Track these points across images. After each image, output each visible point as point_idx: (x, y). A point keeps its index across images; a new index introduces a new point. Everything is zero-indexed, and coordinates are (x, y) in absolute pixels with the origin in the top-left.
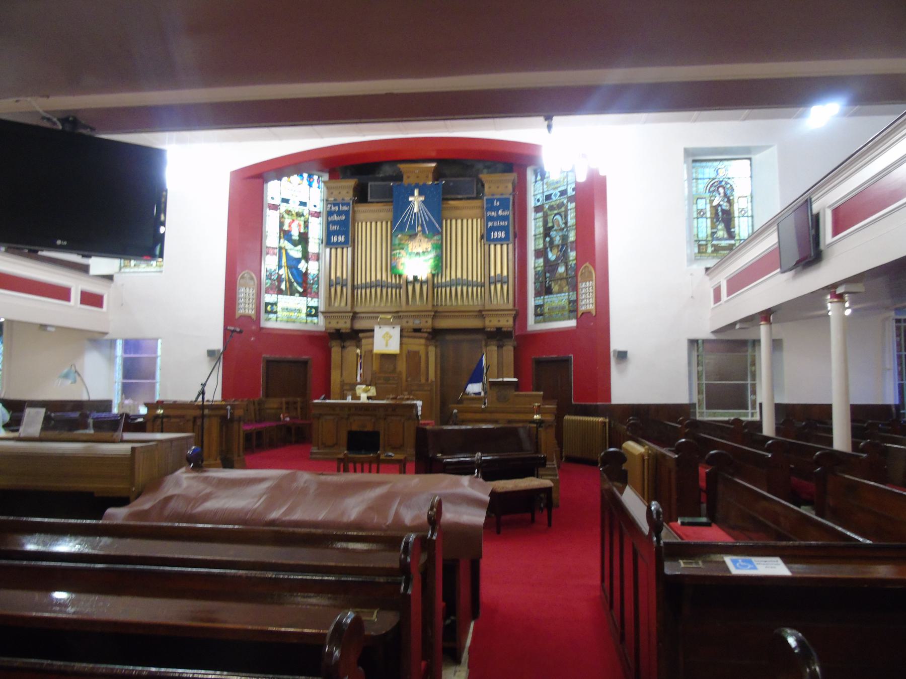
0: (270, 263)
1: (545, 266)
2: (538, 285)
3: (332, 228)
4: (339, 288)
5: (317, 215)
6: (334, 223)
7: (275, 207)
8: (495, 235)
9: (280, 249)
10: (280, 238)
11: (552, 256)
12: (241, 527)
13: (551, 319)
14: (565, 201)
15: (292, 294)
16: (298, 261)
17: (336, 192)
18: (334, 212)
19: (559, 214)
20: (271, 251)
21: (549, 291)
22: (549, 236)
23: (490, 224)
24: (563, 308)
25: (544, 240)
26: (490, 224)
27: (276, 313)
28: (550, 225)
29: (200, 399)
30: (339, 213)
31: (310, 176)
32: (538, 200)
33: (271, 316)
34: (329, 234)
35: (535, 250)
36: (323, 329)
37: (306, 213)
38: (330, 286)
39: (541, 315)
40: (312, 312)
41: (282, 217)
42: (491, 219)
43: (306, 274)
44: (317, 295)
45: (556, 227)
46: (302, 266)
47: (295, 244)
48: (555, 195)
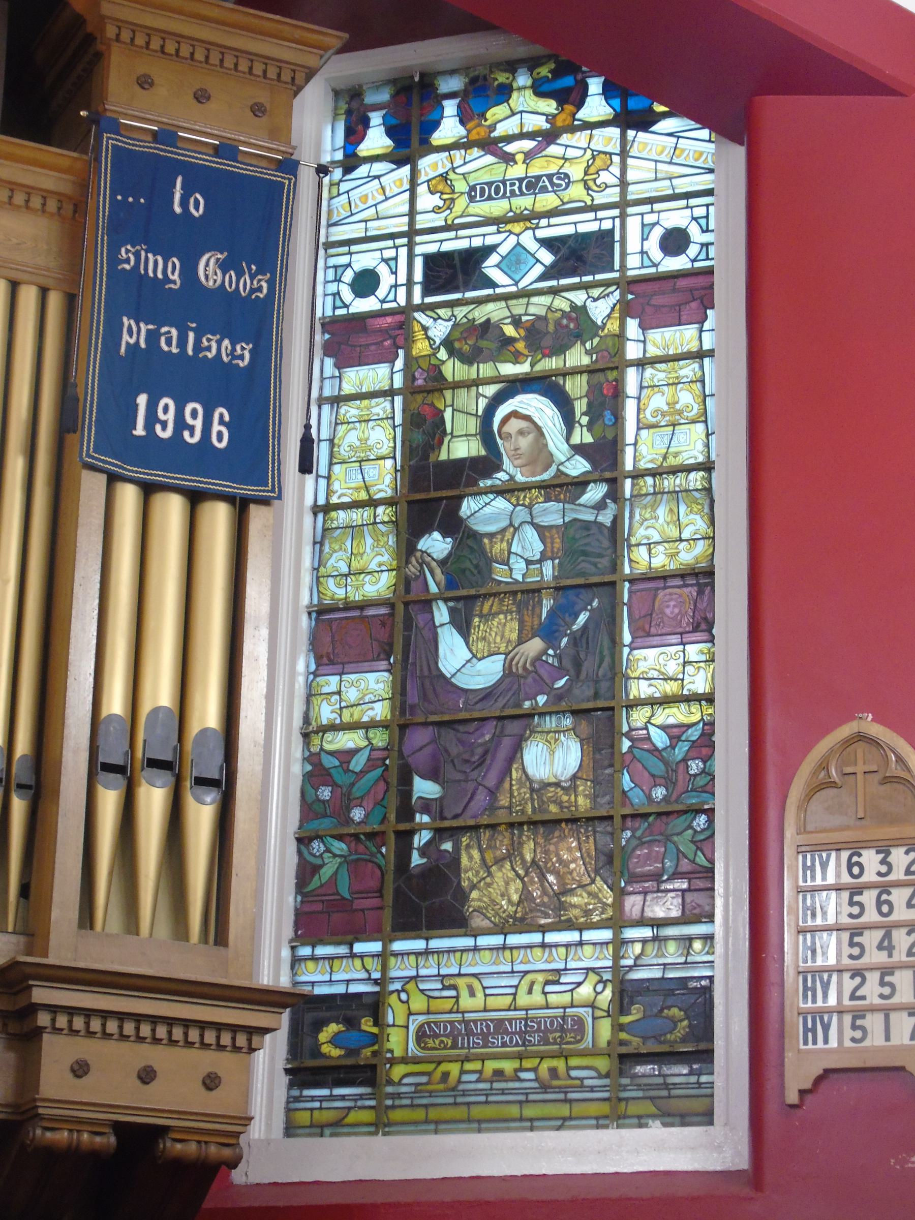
1: (402, 723)
2: (332, 855)
8: (162, 416)
11: (466, 661)
13: (447, 1108)
14: (599, 310)
19: (548, 386)
21: (429, 903)
22: (452, 525)
23: (134, 334)
24: (563, 1033)
25: (407, 549)
26: (134, 334)
28: (462, 448)
29: (456, 1007)
32: (366, 283)
35: (321, 612)
39: (364, 1072)
42: (141, 296)
45: (510, 470)
48: (515, 260)
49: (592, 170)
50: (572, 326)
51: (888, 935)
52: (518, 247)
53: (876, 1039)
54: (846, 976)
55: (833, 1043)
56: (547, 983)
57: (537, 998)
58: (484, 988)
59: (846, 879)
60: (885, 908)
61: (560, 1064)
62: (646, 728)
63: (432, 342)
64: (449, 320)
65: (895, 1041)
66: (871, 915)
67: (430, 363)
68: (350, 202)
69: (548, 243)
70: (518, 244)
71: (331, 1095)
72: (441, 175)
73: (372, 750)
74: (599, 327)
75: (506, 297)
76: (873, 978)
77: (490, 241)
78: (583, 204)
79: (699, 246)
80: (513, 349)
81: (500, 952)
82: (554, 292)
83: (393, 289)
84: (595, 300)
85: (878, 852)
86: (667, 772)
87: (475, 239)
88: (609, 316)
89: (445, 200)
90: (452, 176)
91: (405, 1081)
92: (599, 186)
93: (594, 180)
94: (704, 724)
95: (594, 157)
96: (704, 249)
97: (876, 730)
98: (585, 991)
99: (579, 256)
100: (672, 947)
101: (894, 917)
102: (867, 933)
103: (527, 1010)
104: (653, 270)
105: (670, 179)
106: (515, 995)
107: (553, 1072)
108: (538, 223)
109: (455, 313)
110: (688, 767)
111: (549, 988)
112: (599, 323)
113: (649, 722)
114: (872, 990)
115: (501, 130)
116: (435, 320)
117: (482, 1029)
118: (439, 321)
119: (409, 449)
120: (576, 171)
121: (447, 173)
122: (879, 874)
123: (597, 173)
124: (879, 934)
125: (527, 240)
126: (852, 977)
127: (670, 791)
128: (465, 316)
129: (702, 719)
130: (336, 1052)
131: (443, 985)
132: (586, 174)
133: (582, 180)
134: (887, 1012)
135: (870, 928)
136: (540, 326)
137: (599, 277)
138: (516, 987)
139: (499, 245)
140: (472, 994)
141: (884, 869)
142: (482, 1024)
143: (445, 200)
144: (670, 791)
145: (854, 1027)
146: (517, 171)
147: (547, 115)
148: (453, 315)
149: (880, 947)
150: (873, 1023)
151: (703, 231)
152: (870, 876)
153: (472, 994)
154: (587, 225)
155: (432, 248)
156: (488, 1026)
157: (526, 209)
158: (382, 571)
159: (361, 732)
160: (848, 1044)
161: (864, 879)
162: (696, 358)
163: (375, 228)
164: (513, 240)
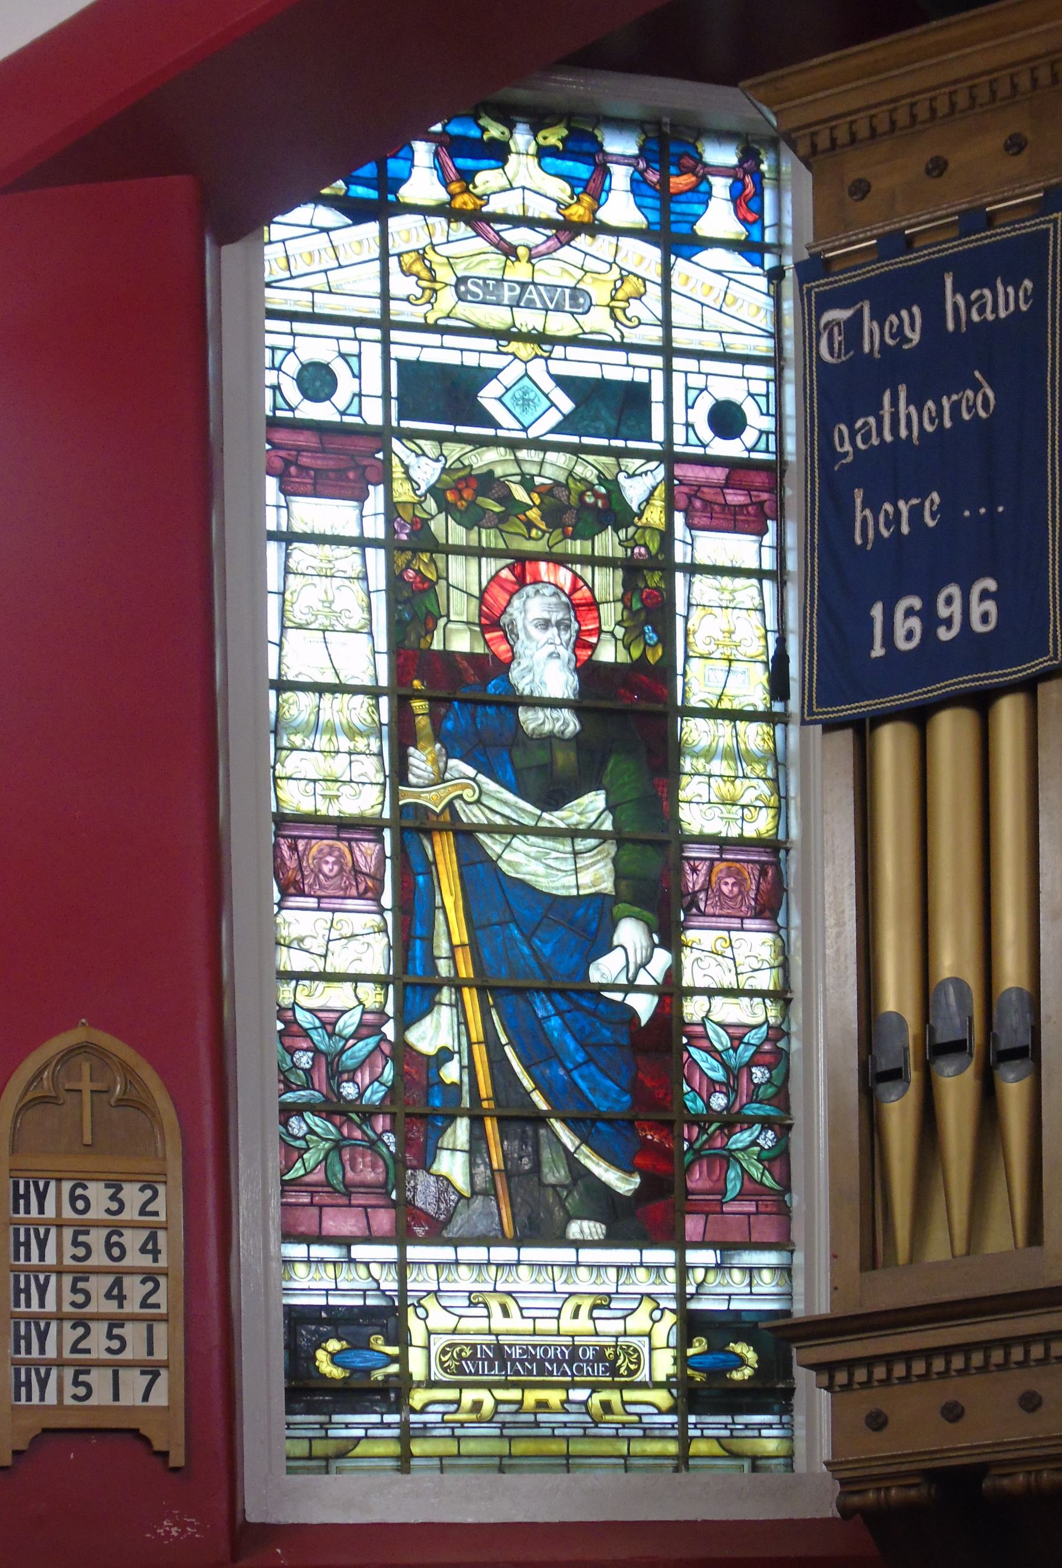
0: (328, 952)
3: (868, 523)
4: (957, 1088)
5: (740, 496)
6: (892, 470)
7: (342, 459)
9: (412, 826)
10: (402, 736)
12: (316, 1398)
14: (634, 492)
15: (538, 1228)
16: (587, 924)
17: (892, 172)
18: (895, 366)
20: (323, 856)
27: (394, 1394)
30: (930, 369)
31: (669, 150)
33: (352, 1424)
34: (839, 590)
36: (819, 1501)
37: (641, 483)
38: (874, 1079)
40: (732, 1368)
41: (409, 543)
43: (663, 1040)
44: (771, 1215)
46: (627, 960)
47: (549, 784)
49: (620, 295)
50: (600, 504)
51: (118, 1283)
52: (526, 379)
53: (101, 1397)
54: (67, 1325)
55: (51, 1398)
56: (594, 1307)
57: (584, 1324)
58: (521, 1309)
59: (68, 1213)
60: (116, 1252)
61: (613, 1396)
62: (704, 1025)
63: (416, 486)
64: (437, 460)
65: (123, 1402)
66: (99, 1258)
67: (415, 516)
68: (287, 257)
69: (564, 382)
70: (526, 374)
71: (382, 1422)
72: (417, 251)
73: (364, 1012)
74: (636, 515)
75: (513, 445)
76: (99, 1329)
77: (490, 361)
78: (610, 339)
79: (757, 434)
80: (522, 517)
81: (573, 1270)
82: (576, 450)
83: (356, 399)
84: (630, 476)
85: (107, 1186)
86: (728, 1079)
87: (473, 353)
88: (648, 501)
89: (424, 289)
90: (430, 255)
91: (431, 1408)
92: (630, 320)
93: (624, 310)
94: (769, 1027)
95: (622, 279)
96: (764, 437)
97: (104, 1039)
98: (639, 1322)
99: (612, 409)
100: (736, 1274)
101: (126, 1262)
102: (93, 1278)
103: (573, 1336)
104: (700, 451)
105: (720, 333)
106: (558, 1318)
107: (606, 1406)
108: (551, 352)
109: (445, 453)
110: (752, 1073)
111: (596, 1313)
112: (635, 509)
113: (706, 1017)
114: (98, 1343)
115: (496, 205)
116: (417, 455)
117: (556, 1354)
118: (424, 459)
119: (397, 627)
120: (600, 292)
121: (424, 249)
122: (108, 1211)
123: (627, 301)
124: (110, 1280)
125: (537, 369)
126: (74, 1327)
127: (732, 1099)
128: (458, 459)
129: (767, 1021)
130: (337, 1373)
131: (471, 1302)
132: (613, 299)
133: (608, 306)
134: (116, 1368)
135: (97, 1273)
136: (562, 494)
137: (461, 429)
138: (560, 1310)
139: (500, 371)
140: (506, 1313)
141: (114, 1206)
142: (556, 1349)
143: (424, 289)
144: (732, 1099)
145: (76, 1383)
146: (520, 271)
147: (558, 203)
148: (442, 454)
149: (108, 1296)
150: (99, 1379)
151: (762, 414)
152: (96, 1213)
153: (506, 1313)
154: (615, 368)
155: (409, 354)
156: (562, 1352)
157: (534, 329)
158: (364, 783)
159: (348, 986)
160: (68, 1401)
161: (91, 1215)
162: (473, 555)
163: (326, 305)
164: (518, 368)
